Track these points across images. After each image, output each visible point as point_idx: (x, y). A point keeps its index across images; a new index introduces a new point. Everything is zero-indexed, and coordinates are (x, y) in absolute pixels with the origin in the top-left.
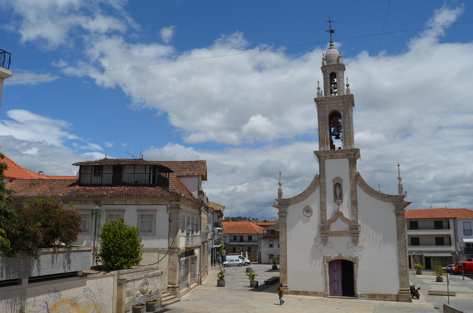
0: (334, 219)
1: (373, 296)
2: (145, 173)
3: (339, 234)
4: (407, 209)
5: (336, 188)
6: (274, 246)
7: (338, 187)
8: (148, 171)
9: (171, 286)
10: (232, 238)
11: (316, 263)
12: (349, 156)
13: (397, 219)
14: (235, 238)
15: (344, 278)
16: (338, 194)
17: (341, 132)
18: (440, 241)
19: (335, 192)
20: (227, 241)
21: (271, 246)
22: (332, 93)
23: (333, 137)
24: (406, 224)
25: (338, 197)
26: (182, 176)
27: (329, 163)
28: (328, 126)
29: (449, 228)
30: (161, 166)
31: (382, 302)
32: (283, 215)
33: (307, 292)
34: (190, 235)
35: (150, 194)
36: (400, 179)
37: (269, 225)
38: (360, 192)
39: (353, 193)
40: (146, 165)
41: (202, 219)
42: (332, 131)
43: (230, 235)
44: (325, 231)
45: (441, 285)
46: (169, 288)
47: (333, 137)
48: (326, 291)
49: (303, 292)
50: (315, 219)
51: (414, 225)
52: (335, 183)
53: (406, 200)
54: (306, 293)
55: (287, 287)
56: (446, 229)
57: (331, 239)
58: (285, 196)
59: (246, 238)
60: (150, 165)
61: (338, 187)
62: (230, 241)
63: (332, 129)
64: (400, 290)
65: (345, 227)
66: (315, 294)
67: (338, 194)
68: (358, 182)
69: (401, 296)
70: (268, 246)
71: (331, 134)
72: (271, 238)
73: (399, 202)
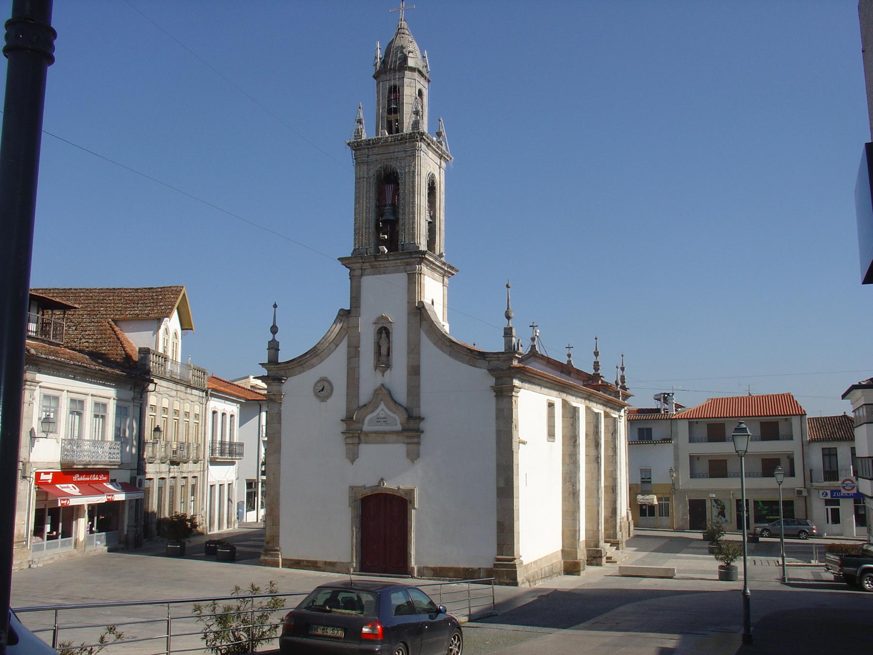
3: (382, 436)
12: (409, 268)
13: (497, 404)
18: (769, 467)
19: (378, 347)
25: (383, 360)
26: (125, 320)
27: (369, 282)
29: (791, 438)
33: (316, 562)
36: (274, 330)
38: (427, 347)
39: (414, 349)
44: (354, 432)
50: (338, 404)
55: (739, 502)
57: (365, 449)
58: (283, 357)
61: (384, 335)
64: (498, 560)
65: (397, 421)
67: (384, 351)
68: (424, 323)
69: (497, 572)
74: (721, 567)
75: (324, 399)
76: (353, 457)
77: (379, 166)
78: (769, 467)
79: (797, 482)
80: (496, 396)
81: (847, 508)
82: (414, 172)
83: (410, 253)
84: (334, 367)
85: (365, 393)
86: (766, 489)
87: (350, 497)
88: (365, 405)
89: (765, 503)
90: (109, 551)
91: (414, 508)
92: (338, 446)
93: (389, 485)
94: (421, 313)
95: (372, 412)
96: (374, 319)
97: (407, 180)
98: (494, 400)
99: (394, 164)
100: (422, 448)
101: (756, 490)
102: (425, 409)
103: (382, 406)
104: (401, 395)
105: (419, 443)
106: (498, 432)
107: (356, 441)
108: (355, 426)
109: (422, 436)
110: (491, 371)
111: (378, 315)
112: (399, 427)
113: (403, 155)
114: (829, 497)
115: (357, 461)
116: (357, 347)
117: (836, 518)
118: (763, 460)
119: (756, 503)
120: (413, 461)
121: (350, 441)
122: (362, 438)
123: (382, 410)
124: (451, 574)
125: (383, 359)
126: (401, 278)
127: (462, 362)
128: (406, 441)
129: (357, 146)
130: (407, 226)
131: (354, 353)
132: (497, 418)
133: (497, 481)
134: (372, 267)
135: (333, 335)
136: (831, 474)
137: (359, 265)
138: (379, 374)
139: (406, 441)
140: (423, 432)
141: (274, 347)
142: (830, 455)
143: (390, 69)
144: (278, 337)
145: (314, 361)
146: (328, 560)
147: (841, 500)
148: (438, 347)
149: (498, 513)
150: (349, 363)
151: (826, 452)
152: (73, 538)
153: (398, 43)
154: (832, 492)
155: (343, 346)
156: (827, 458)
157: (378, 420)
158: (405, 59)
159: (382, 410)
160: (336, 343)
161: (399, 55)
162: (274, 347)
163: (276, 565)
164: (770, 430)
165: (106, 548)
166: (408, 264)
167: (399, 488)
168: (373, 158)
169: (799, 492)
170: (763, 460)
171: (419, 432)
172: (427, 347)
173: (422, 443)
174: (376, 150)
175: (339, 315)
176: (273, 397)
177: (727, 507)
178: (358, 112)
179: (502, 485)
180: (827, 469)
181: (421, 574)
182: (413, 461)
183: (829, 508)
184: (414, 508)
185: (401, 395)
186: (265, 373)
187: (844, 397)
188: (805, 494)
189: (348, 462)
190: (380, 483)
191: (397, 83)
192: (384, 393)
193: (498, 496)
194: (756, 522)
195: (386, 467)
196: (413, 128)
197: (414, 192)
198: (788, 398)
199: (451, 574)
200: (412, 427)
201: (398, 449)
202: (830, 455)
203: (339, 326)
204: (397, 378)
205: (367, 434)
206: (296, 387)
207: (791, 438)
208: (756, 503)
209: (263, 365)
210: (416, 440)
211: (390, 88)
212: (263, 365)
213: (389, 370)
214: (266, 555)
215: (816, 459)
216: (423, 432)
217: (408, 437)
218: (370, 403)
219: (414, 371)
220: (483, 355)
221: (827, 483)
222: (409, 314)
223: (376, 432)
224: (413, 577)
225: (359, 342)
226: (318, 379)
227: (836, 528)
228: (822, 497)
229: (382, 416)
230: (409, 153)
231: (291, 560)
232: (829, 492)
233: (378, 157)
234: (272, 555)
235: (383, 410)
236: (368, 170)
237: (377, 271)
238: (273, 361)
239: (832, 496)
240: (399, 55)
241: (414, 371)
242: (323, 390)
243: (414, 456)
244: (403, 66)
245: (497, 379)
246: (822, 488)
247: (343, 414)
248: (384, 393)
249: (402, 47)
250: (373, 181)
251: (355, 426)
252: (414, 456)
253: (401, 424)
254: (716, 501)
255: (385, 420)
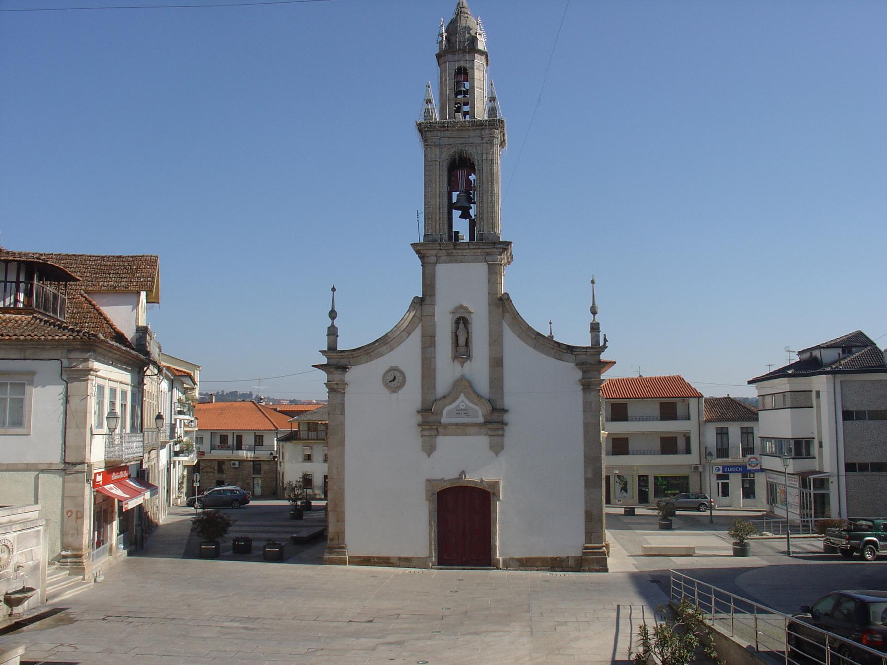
0: (450, 397)
1: (526, 564)
2: (6, 282)
3: (461, 429)
4: (607, 375)
5: (457, 328)
6: (314, 458)
7: (461, 325)
8: (12, 277)
9: (69, 553)
10: (217, 442)
11: (840, 514)
12: (489, 258)
13: (585, 397)
14: (224, 439)
15: (463, 527)
16: (462, 341)
17: (474, 203)
18: (669, 445)
20: (206, 446)
21: (308, 458)
22: (458, 110)
23: (456, 213)
24: (603, 406)
25: (462, 350)
27: (445, 271)
28: (446, 188)
29: (688, 418)
30: (45, 264)
31: (548, 574)
32: (335, 389)
33: (388, 558)
34: (118, 431)
35: (18, 332)
36: (333, 314)
37: (305, 411)
38: (511, 339)
39: (496, 341)
40: (7, 262)
41: (146, 394)
42: (454, 200)
43: (213, 433)
44: (430, 420)
45: (673, 535)
46: (64, 557)
47: (456, 213)
48: (430, 557)
49: (400, 558)
50: (412, 394)
51: (619, 413)
52: (458, 316)
53: (604, 357)
54: (386, 562)
56: (682, 419)
57: (443, 442)
59: (231, 441)
60: (19, 262)
61: (461, 325)
62: (213, 448)
63: (455, 194)
64: (587, 548)
65: (479, 413)
66: (406, 562)
67: (462, 341)
69: (587, 560)
70: (300, 458)
71: (451, 207)
72: (308, 439)
73: (589, 361)
74: (735, 544)
75: (395, 390)
76: (430, 449)
77: (453, 150)
78: (669, 445)
79: (693, 459)
80: (584, 390)
81: (735, 482)
82: (492, 160)
83: (494, 243)
84: (407, 356)
85: (443, 385)
86: (665, 466)
87: (427, 491)
88: (444, 397)
89: (664, 478)
90: (129, 554)
91: (499, 500)
92: (413, 438)
93: (473, 478)
94: (503, 306)
95: (451, 403)
96: (451, 307)
97: (485, 168)
98: (581, 393)
99: (470, 151)
100: (507, 440)
101: (658, 467)
102: (508, 401)
103: (462, 397)
104: (483, 385)
105: (503, 435)
106: (586, 425)
107: (434, 433)
108: (432, 418)
109: (506, 428)
110: (580, 364)
111: (458, 304)
112: (481, 420)
113: (479, 141)
114: (721, 472)
115: (435, 454)
116: (433, 337)
117: (725, 491)
118: (662, 439)
119: (656, 478)
120: (497, 453)
121: (427, 433)
122: (440, 430)
123: (462, 401)
124: (539, 563)
125: (462, 349)
126: (481, 269)
127: (547, 355)
128: (490, 433)
129: (425, 129)
130: (485, 215)
131: (429, 342)
132: (585, 411)
133: (586, 472)
134: (449, 255)
135: (406, 323)
136: (723, 451)
137: (434, 252)
138: (457, 364)
139: (490, 433)
140: (506, 424)
141: (332, 332)
142: (722, 434)
143: (460, 50)
144: (336, 323)
145: (384, 349)
146: (403, 556)
147: (731, 475)
148: (521, 339)
149: (586, 503)
150: (423, 353)
151: (719, 431)
152: (108, 545)
153: (463, 23)
154: (724, 467)
155: (417, 333)
156: (720, 437)
157: (458, 412)
158: (474, 40)
159: (462, 401)
160: (408, 331)
161: (467, 36)
162: (332, 332)
163: (344, 563)
164: (668, 412)
165: (126, 551)
166: (488, 254)
167: (482, 481)
168: (446, 141)
169: (696, 468)
170: (662, 439)
171: (503, 423)
172: (511, 339)
173: (506, 435)
174: (448, 133)
175: (414, 302)
176: (335, 387)
177: (629, 480)
178: (427, 92)
179: (590, 475)
180: (720, 447)
181: (507, 565)
182: (497, 453)
183: (721, 482)
184: (499, 500)
185: (483, 385)
186: (324, 360)
187: (750, 382)
188: (701, 470)
189: (424, 454)
190: (461, 475)
191: (468, 65)
192: (463, 385)
193: (586, 487)
194: (656, 496)
195: (465, 459)
196: (490, 115)
197: (492, 180)
198: (678, 381)
199: (539, 563)
200: (495, 420)
201: (481, 442)
202: (722, 434)
203: (412, 314)
204: (478, 369)
205: (446, 426)
206: (363, 379)
207: (688, 418)
208: (656, 478)
209: (323, 352)
210: (500, 433)
211: (459, 69)
212: (323, 352)
213: (469, 361)
214: (330, 553)
215: (711, 438)
216: (506, 424)
217: (492, 429)
218: (449, 394)
219: (497, 363)
220: (571, 349)
221: (720, 460)
222: (490, 305)
223: (457, 424)
224: (498, 569)
225: (434, 330)
226: (387, 368)
227: (725, 500)
228: (715, 472)
229: (462, 408)
230: (486, 140)
231: (359, 557)
232: (721, 468)
233: (451, 140)
234: (338, 553)
235: (463, 402)
236: (441, 153)
237: (452, 258)
238: (332, 348)
239: (724, 472)
240: (467, 36)
241: (497, 363)
242: (394, 380)
243: (497, 448)
244: (472, 47)
245: (584, 372)
246: (715, 464)
247: (418, 405)
248: (463, 385)
249: (469, 29)
250: (446, 165)
251: (432, 418)
252: (497, 448)
253: (484, 416)
254: (619, 477)
255: (466, 412)
